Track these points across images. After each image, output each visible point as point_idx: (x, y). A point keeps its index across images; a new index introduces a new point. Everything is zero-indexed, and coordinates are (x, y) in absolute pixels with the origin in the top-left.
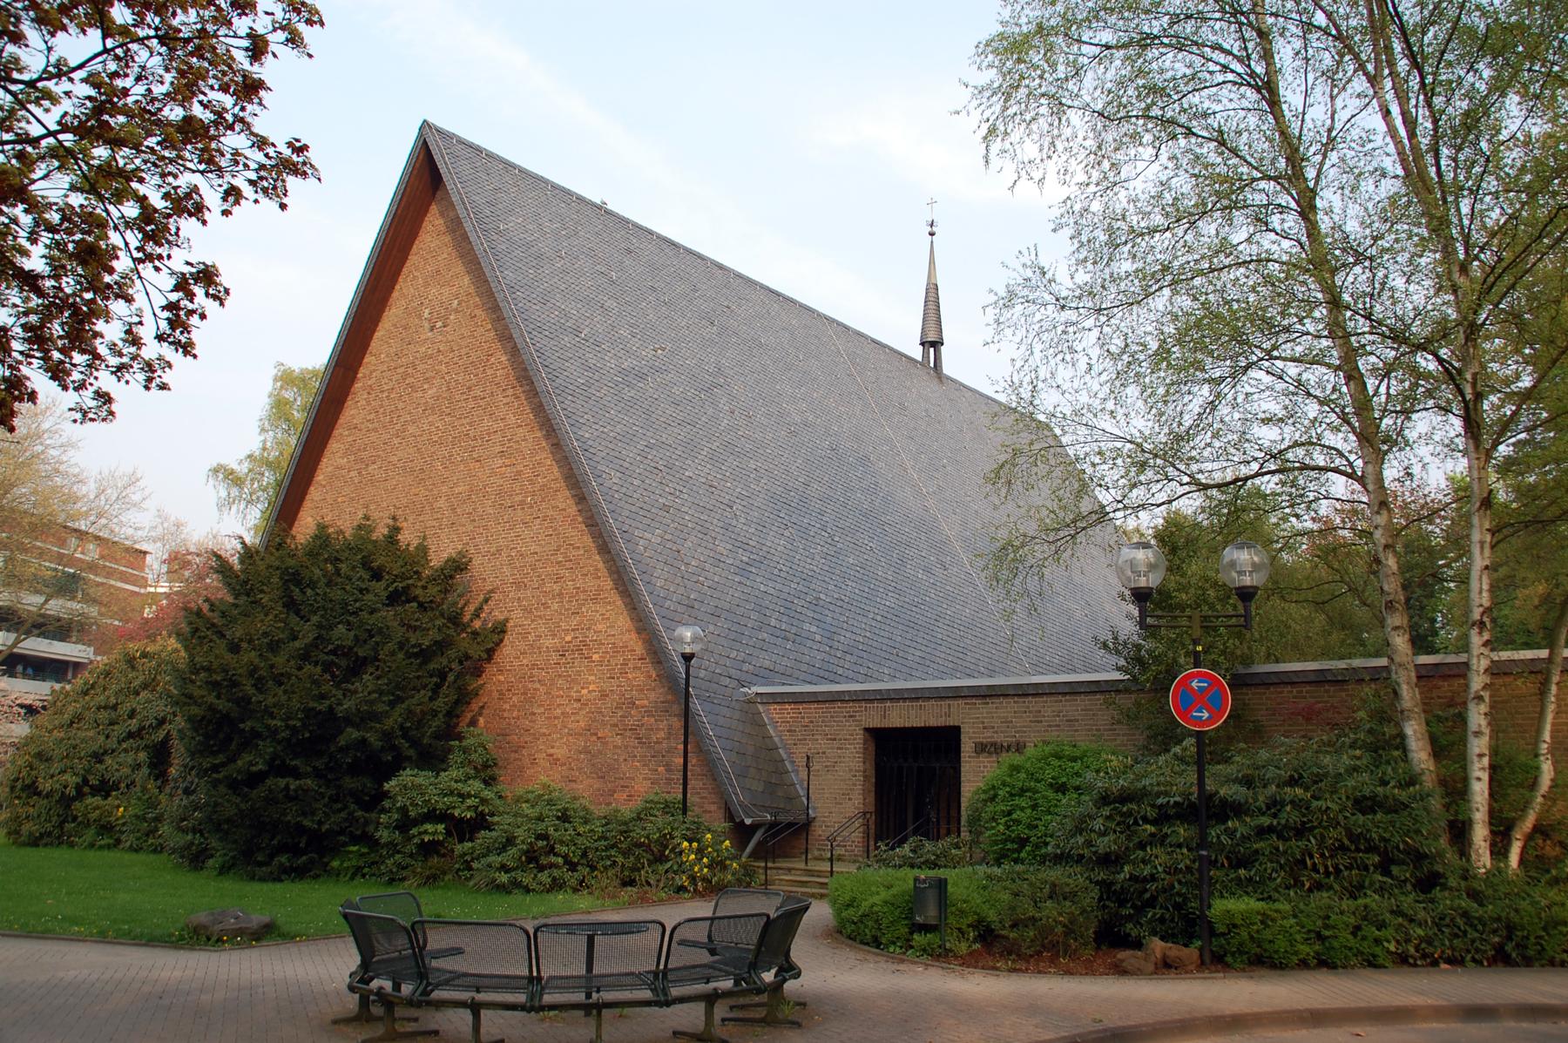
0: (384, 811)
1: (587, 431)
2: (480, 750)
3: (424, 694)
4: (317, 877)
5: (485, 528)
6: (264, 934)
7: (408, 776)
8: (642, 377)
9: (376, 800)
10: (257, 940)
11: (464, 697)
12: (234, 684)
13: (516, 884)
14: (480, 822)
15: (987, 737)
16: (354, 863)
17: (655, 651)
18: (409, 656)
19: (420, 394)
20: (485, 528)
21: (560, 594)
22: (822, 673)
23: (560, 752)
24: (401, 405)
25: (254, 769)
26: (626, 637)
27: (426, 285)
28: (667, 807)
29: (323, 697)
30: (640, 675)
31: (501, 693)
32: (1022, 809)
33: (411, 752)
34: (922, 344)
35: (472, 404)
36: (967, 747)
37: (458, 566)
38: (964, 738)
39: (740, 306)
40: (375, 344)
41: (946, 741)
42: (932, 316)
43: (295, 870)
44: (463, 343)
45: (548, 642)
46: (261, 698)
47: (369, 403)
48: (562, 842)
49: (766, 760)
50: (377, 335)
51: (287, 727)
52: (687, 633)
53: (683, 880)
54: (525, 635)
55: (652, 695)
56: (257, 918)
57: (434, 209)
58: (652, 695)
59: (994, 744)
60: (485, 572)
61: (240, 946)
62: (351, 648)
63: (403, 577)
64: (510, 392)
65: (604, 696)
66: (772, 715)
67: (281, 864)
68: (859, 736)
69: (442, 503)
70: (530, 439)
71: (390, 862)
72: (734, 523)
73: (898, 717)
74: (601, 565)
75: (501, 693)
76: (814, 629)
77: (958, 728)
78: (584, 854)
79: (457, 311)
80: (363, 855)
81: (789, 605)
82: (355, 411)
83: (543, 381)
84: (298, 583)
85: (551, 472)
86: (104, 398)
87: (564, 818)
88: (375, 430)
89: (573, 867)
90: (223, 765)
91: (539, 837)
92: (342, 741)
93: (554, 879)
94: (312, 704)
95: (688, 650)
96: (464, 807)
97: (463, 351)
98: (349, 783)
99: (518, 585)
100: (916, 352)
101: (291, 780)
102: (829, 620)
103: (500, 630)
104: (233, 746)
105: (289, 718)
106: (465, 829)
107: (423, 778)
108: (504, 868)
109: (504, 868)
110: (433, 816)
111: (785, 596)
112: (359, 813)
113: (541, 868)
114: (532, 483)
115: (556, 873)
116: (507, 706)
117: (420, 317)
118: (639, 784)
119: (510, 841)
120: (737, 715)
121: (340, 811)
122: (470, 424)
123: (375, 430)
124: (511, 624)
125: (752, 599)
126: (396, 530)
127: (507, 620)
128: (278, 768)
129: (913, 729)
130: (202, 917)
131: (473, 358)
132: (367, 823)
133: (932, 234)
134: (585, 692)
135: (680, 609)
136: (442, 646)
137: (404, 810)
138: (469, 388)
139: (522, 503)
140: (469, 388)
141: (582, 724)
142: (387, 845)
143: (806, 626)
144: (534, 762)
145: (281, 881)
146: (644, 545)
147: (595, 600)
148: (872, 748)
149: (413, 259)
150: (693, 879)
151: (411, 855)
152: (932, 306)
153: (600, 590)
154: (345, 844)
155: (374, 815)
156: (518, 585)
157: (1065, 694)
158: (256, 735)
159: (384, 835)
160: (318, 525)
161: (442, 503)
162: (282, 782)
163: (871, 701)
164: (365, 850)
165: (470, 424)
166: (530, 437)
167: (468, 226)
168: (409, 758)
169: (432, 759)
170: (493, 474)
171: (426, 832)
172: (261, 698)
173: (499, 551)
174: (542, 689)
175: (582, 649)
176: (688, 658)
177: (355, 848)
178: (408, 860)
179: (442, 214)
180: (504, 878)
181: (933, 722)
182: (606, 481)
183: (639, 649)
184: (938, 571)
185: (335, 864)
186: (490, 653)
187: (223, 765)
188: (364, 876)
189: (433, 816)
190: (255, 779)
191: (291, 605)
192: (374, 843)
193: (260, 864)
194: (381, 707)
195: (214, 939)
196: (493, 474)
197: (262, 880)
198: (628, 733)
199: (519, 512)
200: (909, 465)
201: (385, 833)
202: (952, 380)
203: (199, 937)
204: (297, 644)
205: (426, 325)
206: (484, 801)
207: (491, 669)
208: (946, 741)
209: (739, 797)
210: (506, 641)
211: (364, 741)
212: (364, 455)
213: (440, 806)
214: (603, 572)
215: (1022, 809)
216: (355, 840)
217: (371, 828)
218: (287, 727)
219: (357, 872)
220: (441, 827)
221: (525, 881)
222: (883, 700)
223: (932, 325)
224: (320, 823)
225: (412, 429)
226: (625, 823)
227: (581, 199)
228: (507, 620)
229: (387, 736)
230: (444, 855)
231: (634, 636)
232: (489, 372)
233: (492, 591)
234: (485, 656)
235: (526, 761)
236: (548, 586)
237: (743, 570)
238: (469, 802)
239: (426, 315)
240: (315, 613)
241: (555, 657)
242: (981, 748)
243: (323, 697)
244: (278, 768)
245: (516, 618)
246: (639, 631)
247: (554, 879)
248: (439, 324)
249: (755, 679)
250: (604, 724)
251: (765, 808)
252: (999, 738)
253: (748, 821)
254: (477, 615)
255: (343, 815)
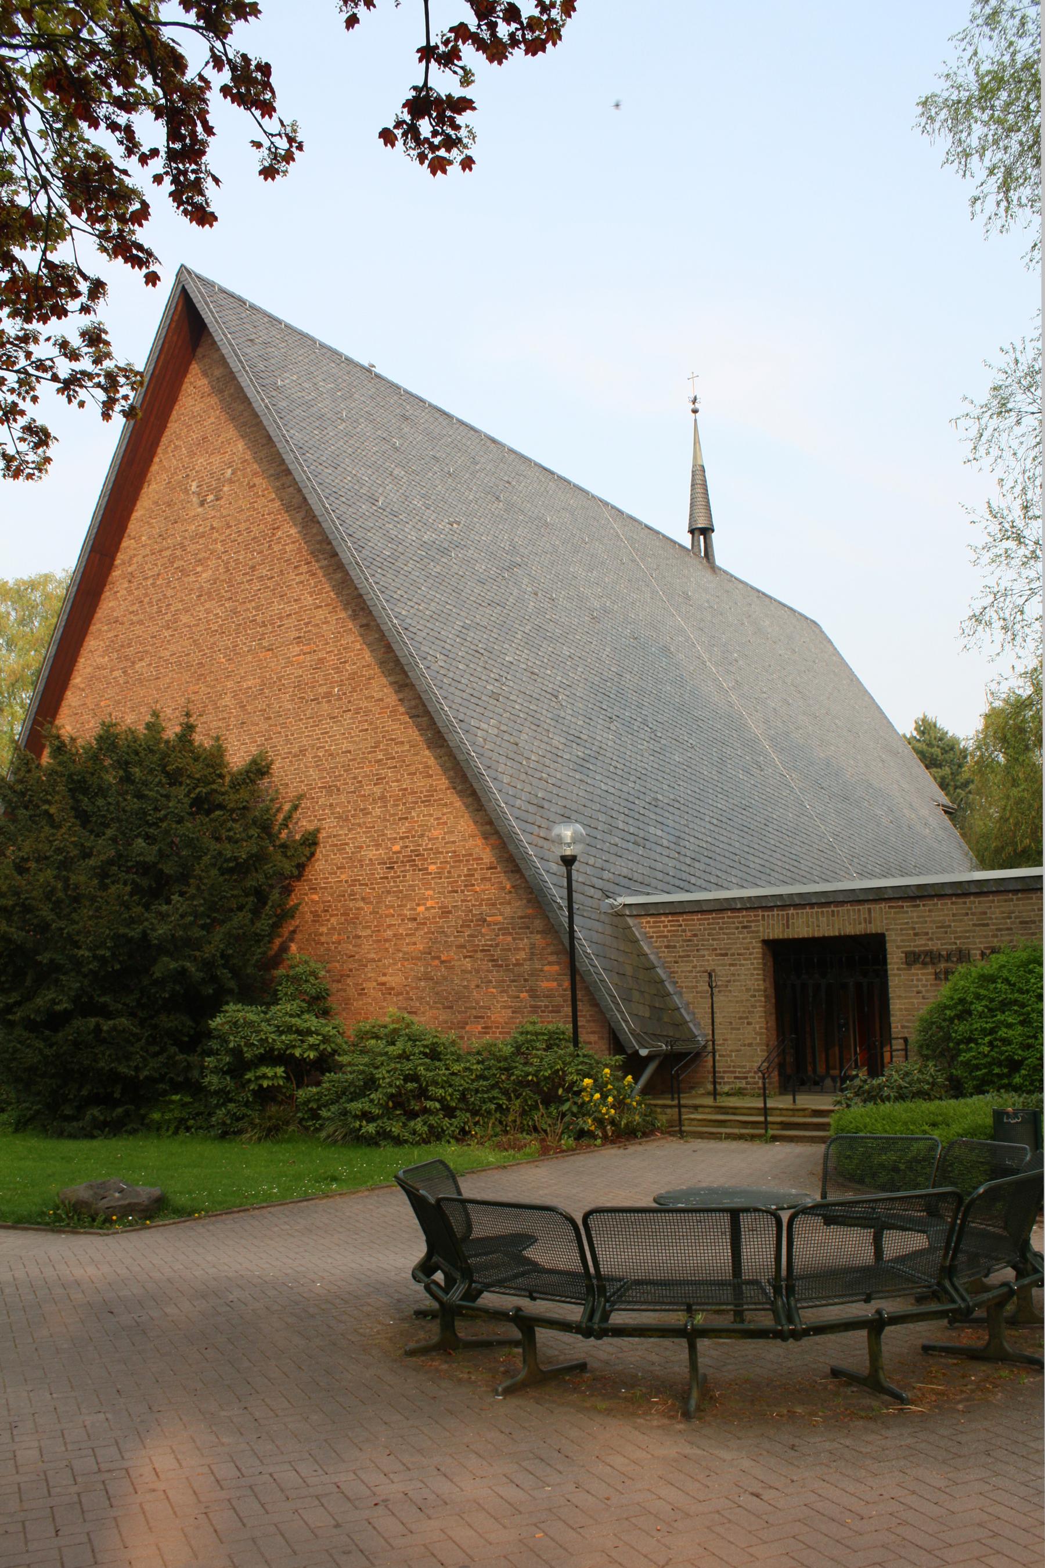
0: (210, 1053)
1: (401, 609)
2: (312, 979)
3: (241, 918)
4: (133, 1132)
5: (284, 726)
6: (154, 1211)
7: (235, 1011)
8: (444, 552)
9: (197, 1040)
10: (150, 1218)
11: (285, 914)
12: (27, 909)
13: (384, 1135)
14: (325, 1063)
15: (920, 944)
16: (177, 1114)
17: (510, 860)
18: (223, 872)
19: (192, 578)
20: (284, 726)
21: (382, 798)
22: (677, 882)
23: (393, 980)
24: (170, 593)
25: (58, 1008)
26: (471, 842)
27: (192, 454)
28: (552, 1041)
29: (131, 922)
30: (491, 888)
31: (315, 914)
32: (1009, 1026)
33: (232, 984)
34: (692, 531)
35: (257, 586)
36: (895, 957)
37: (259, 769)
38: (890, 947)
39: (519, 482)
40: (133, 526)
41: (866, 954)
42: (700, 499)
43: (105, 1124)
44: (242, 517)
45: (371, 853)
46: (62, 924)
47: (130, 592)
48: (435, 1083)
49: (647, 983)
50: (136, 515)
51: (95, 957)
52: (567, 832)
53: (589, 1124)
54: (341, 848)
55: (508, 910)
56: (145, 1192)
57: (195, 368)
58: (508, 910)
59: (929, 953)
60: (288, 778)
61: (132, 1228)
62: (155, 864)
63: (204, 781)
64: (304, 568)
65: (445, 912)
66: (641, 927)
67: (94, 1118)
68: (757, 950)
69: (227, 700)
70: (334, 624)
71: (221, 1113)
72: (563, 714)
73: (804, 926)
74: (432, 762)
75: (315, 914)
76: (659, 833)
77: (883, 935)
78: (463, 1098)
79: (231, 481)
80: (184, 1105)
81: (632, 806)
82: (113, 603)
83: (348, 553)
84: (85, 791)
85: (362, 657)
86: (40, 436)
87: (434, 1054)
88: (141, 622)
89: (449, 1112)
90: (18, 1004)
91: (407, 1079)
92: (157, 972)
93: (431, 1127)
94: (122, 930)
95: (568, 852)
96: (305, 1045)
97: (243, 526)
98: (167, 1021)
99: (330, 789)
100: (685, 540)
101: (101, 1021)
102: (671, 823)
103: (311, 841)
104: (28, 983)
105: (98, 948)
106: (307, 1071)
107: (250, 1014)
108: (366, 1116)
109: (366, 1116)
110: (271, 1057)
111: (625, 796)
112: (180, 1057)
113: (413, 1115)
114: (338, 670)
115: (432, 1120)
116: (324, 930)
117: (186, 491)
118: (499, 1015)
119: (371, 1083)
120: (609, 930)
121: (156, 1055)
122: (257, 608)
123: (141, 622)
124: (323, 834)
125: (596, 799)
126: (190, 728)
127: (318, 830)
128: (85, 1007)
129: (824, 939)
130: (80, 1190)
131: (255, 531)
132: (189, 1067)
133: (695, 411)
134: (421, 909)
135: (532, 809)
136: (259, 859)
137: (237, 1052)
138: (253, 568)
139: (328, 695)
140: (253, 568)
141: (421, 947)
142: (216, 1093)
143: (652, 830)
144: (362, 993)
145: (93, 1137)
146: (479, 736)
147: (427, 802)
148: (770, 964)
149: (173, 426)
150: (600, 1122)
151: (247, 1104)
152: (699, 490)
153: (432, 790)
154: (165, 1093)
155: (194, 1059)
156: (330, 789)
157: (1016, 892)
158: (55, 967)
159: (213, 1081)
160: (103, 724)
161: (227, 700)
162: (93, 1021)
163: (771, 908)
164: (188, 1099)
165: (257, 608)
166: (333, 619)
167: (244, 380)
168: (230, 991)
169: (258, 990)
170: (289, 663)
171: (265, 1076)
172: (62, 924)
173: (303, 751)
174: (367, 908)
175: (414, 860)
176: (568, 861)
177: (176, 1097)
178: (244, 1110)
179: (205, 374)
180: (371, 1128)
181: (850, 930)
182: (432, 667)
183: (488, 856)
184: (755, 771)
185: (156, 1116)
186: (301, 867)
187: (18, 1004)
188: (188, 1129)
189: (271, 1057)
190: (55, 1021)
191: (83, 818)
192: (197, 1089)
193: (67, 1119)
194: (197, 933)
195: (100, 1218)
196: (289, 663)
197: (72, 1136)
198: (479, 955)
199: (325, 706)
200: (705, 657)
201: (215, 1079)
202: (725, 572)
203: (78, 1216)
204: (92, 862)
205: (195, 500)
206: (326, 1039)
207: (301, 888)
208: (866, 954)
209: (627, 1025)
210: (318, 855)
211: (183, 972)
212: (130, 651)
213: (278, 1045)
214: (435, 768)
215: (1009, 1026)
216: (176, 1088)
217: (195, 1074)
218: (95, 957)
219: (181, 1126)
220: (280, 1070)
221: (396, 1130)
222: (783, 907)
223: (700, 511)
224: (137, 1069)
225: (185, 619)
226: (506, 1059)
227: (349, 360)
228: (318, 830)
229: (208, 965)
230: (281, 1103)
231: (479, 841)
232: (276, 548)
233: (300, 797)
234: (296, 873)
235: (352, 992)
236: (367, 789)
237: (581, 765)
238: (311, 1040)
239: (194, 488)
240: (107, 826)
241: (380, 871)
242: (913, 959)
243: (131, 922)
244: (85, 1007)
245: (329, 826)
246: (486, 837)
247: (431, 1127)
248: (210, 498)
249: (617, 889)
250: (448, 946)
251: (657, 1037)
252: (935, 946)
253: (644, 1052)
254: (285, 825)
255: (162, 1058)
